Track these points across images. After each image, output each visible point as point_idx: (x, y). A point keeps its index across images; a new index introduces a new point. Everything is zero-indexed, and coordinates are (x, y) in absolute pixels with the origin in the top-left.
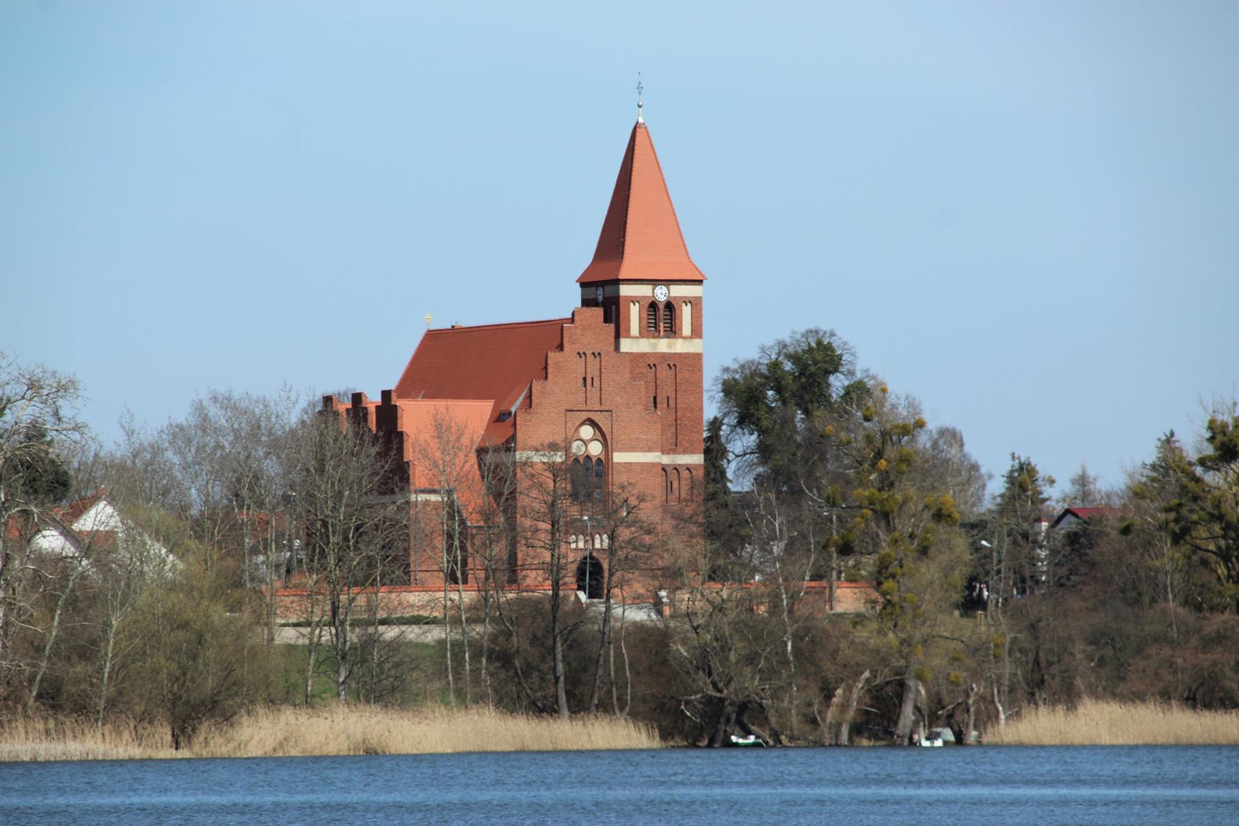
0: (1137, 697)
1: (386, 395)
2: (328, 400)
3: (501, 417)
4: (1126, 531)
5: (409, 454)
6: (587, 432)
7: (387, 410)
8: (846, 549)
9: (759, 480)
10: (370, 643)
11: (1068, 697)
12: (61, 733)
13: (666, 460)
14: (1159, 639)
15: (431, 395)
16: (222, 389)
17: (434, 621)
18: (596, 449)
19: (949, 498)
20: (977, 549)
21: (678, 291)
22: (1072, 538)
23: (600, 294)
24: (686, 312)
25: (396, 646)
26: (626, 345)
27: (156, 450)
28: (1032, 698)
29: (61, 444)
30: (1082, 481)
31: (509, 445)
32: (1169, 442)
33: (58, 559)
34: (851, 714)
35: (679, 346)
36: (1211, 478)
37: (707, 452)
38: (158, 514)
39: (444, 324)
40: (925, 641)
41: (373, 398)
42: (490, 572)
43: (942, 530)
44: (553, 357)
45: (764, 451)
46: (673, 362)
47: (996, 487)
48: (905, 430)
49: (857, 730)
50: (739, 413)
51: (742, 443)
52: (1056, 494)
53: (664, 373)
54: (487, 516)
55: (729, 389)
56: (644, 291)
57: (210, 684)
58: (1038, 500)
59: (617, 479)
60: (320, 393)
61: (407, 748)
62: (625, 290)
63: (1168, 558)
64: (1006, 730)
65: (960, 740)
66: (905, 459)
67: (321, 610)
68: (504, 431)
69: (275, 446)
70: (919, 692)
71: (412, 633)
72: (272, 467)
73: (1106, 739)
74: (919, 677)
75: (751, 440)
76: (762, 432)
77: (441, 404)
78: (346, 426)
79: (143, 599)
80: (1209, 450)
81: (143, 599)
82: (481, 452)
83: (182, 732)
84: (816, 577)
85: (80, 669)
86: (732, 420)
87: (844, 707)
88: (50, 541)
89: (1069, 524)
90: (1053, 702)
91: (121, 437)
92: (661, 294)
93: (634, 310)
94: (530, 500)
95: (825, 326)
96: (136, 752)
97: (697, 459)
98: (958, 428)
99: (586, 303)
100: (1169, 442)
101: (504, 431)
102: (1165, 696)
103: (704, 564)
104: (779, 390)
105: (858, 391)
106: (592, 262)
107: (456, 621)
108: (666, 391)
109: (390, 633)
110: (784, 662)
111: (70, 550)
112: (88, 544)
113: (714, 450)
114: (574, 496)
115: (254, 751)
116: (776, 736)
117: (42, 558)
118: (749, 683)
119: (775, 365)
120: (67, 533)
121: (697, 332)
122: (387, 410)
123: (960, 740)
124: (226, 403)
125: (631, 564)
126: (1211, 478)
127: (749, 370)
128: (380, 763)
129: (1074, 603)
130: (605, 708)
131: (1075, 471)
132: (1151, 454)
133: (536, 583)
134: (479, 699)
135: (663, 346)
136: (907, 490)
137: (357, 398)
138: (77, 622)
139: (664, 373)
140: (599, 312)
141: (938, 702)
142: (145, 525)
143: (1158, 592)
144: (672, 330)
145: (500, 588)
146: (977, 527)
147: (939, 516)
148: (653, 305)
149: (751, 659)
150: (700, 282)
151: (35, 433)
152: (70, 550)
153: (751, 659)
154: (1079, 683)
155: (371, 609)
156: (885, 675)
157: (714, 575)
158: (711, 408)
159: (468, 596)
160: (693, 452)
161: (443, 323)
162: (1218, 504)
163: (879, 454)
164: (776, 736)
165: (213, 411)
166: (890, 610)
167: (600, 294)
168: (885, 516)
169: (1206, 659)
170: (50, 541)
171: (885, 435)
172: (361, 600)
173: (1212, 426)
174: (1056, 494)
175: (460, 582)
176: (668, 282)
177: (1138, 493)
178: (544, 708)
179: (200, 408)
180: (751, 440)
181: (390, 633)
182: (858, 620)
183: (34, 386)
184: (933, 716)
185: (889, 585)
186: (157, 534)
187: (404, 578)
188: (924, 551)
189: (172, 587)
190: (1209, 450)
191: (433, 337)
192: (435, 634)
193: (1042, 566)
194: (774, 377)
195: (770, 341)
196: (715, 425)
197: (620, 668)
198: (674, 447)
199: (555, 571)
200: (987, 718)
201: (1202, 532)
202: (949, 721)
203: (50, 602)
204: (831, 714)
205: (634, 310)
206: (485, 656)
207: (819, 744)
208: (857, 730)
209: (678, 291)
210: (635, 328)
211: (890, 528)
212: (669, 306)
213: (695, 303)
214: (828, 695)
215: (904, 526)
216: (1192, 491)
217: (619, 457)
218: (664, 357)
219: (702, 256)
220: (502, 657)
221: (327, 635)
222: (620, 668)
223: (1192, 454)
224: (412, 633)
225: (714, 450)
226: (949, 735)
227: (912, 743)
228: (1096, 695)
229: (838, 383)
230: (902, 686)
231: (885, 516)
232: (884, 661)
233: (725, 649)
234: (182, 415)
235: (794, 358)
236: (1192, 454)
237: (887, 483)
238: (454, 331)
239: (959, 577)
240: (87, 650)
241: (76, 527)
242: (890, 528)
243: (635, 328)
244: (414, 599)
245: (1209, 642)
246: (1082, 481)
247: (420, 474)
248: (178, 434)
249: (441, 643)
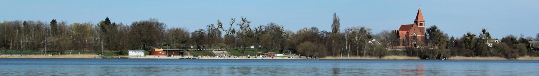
0: (460, 56)
1: (398, 30)
2: (393, 31)
3: (407, 32)
5: (400, 35)
6: (415, 33)
7: (398, 32)
8: (436, 43)
9: (429, 38)
10: (396, 50)
11: (455, 56)
12: (370, 57)
13: (421, 36)
14: (463, 51)
15: (402, 30)
16: (384, 30)
17: (401, 49)
18: (415, 35)
20: (447, 43)
21: (422, 22)
22: (456, 43)
24: (423, 24)
25: (398, 51)
26: (418, 26)
28: (452, 56)
29: (371, 34)
30: (457, 38)
31: (408, 34)
32: (465, 34)
33: (370, 43)
35: (423, 27)
37: (425, 35)
39: (403, 25)
40: (443, 51)
41: (397, 31)
42: (406, 45)
43: (444, 42)
44: (412, 27)
45: (430, 35)
46: (422, 28)
47: (450, 38)
48: (441, 34)
49: (437, 58)
50: (209, 56)
51: (428, 35)
52: (455, 39)
53: (421, 29)
54: (406, 40)
55: (427, 30)
56: (420, 22)
57: (382, 53)
58: (453, 39)
59: (417, 37)
60: (392, 30)
61: (399, 59)
62: (418, 22)
63: (464, 44)
64: (450, 58)
65: (446, 59)
66: (441, 36)
67: (392, 48)
68: (408, 33)
69: (388, 34)
70: (442, 55)
72: (388, 36)
74: (442, 54)
75: (429, 34)
76: (430, 34)
79: (377, 47)
80: (467, 35)
81: (377, 47)
82: (406, 35)
85: (372, 52)
86: (427, 33)
87: (436, 56)
88: (370, 42)
89: (456, 42)
90: (454, 56)
92: (421, 22)
93: (419, 24)
94: (410, 39)
95: (435, 25)
97: (424, 36)
99: (415, 23)
100: (465, 34)
101: (408, 33)
102: (463, 56)
103: (424, 45)
104: (431, 30)
105: (438, 31)
107: (403, 49)
108: (421, 30)
109: (397, 50)
110: (431, 52)
111: (371, 42)
112: (373, 42)
113: (426, 35)
116: (430, 59)
117: (369, 43)
118: (428, 54)
119: (431, 28)
120: (371, 41)
121: (424, 25)
122: (398, 32)
123: (446, 59)
124: (384, 31)
125: (418, 44)
128: (130, 39)
129: (455, 48)
130: (415, 56)
131: (456, 37)
132: (463, 36)
133: (410, 46)
134: (405, 55)
135: (421, 27)
136: (441, 39)
137: (395, 31)
138: (372, 48)
139: (421, 29)
140: (416, 24)
143: (463, 47)
144: (422, 25)
145: (407, 46)
146: (448, 42)
147: (444, 41)
148: (420, 23)
149: (428, 52)
150: (424, 21)
152: (371, 42)
154: (456, 55)
155: (396, 48)
156: (439, 54)
157: (425, 45)
158: (425, 32)
159: (404, 47)
163: (439, 36)
164: (430, 59)
165: (383, 32)
166: (440, 48)
168: (439, 41)
169: (467, 53)
170: (370, 42)
171: (440, 34)
172: (395, 47)
174: (455, 39)
176: (422, 21)
177: (461, 39)
178: (410, 56)
179: (382, 31)
180: (429, 34)
181: (397, 50)
182: (437, 49)
183: (368, 29)
184: (443, 57)
186: (379, 41)
187: (399, 45)
190: (467, 35)
191: (402, 26)
192: (401, 50)
194: (431, 29)
195: (430, 26)
196: (426, 33)
197: (417, 53)
198: (422, 35)
199: (411, 45)
202: (445, 58)
204: (434, 57)
205: (419, 24)
206: (334, 51)
207: (433, 59)
208: (437, 58)
211: (440, 42)
212: (422, 23)
213: (424, 23)
214: (434, 55)
215: (441, 42)
216: (466, 39)
217: (417, 36)
218: (421, 27)
219: (424, 19)
220: (407, 52)
222: (417, 53)
223: (466, 36)
224: (399, 50)
225: (426, 35)
226: (445, 59)
229: (436, 30)
230: (441, 55)
231: (439, 41)
232: (439, 53)
233: (426, 51)
235: (433, 28)
236: (466, 36)
237: (440, 38)
238: (404, 25)
239: (446, 46)
240: (372, 51)
241: (372, 41)
242: (440, 42)
244: (400, 47)
246: (457, 38)
247: (400, 37)
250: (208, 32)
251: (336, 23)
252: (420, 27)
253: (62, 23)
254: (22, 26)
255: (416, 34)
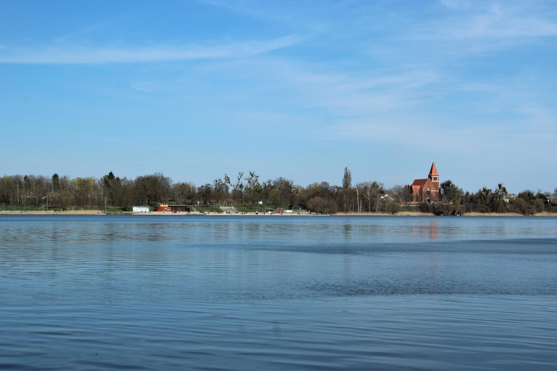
0: (476, 212)
1: (411, 185)
2: (406, 186)
3: (421, 187)
4: (476, 197)
5: (413, 190)
6: (428, 188)
7: (411, 187)
8: (451, 199)
9: (444, 193)
11: (470, 212)
13: (435, 191)
14: (478, 207)
16: (397, 184)
18: (429, 190)
19: (460, 195)
20: (462, 199)
21: (437, 176)
22: (471, 198)
23: (430, 177)
24: (437, 178)
25: (411, 206)
26: (432, 181)
27: (391, 190)
29: (383, 189)
30: (472, 193)
31: (422, 190)
33: (383, 199)
34: (451, 213)
35: (437, 181)
36: (483, 193)
38: (392, 195)
39: (416, 179)
41: (410, 185)
43: (459, 197)
44: (426, 182)
45: (444, 190)
46: (436, 183)
47: (465, 194)
48: (456, 189)
49: (451, 214)
51: (442, 190)
52: (470, 194)
53: (435, 184)
54: (419, 196)
55: (441, 185)
56: (434, 176)
57: (395, 209)
58: (469, 195)
59: (431, 192)
60: (405, 185)
62: (432, 176)
63: (479, 200)
64: (465, 214)
65: (460, 215)
67: (405, 203)
69: (401, 189)
71: (413, 205)
72: (401, 191)
73: (473, 215)
74: (457, 210)
75: (443, 189)
76: (444, 189)
77: (416, 186)
78: (407, 188)
79: (390, 202)
80: (483, 191)
81: (390, 202)
82: (419, 190)
83: (393, 213)
84: (448, 201)
86: (441, 188)
87: (450, 212)
88: (382, 197)
89: (471, 197)
90: (469, 212)
91: (388, 188)
92: (435, 177)
93: (433, 178)
94: (423, 194)
95: (450, 180)
96: (389, 215)
97: (438, 191)
98: (139, 176)
99: (429, 177)
103: (438, 200)
105: (452, 185)
106: (430, 174)
107: (416, 205)
108: (435, 185)
109: (411, 205)
110: (445, 208)
111: (384, 198)
112: (385, 197)
114: (427, 194)
115: (399, 215)
117: (381, 199)
118: (442, 210)
119: (445, 183)
120: (384, 196)
121: (438, 180)
122: (411, 187)
123: (460, 215)
124: (397, 186)
125: (432, 200)
126: (483, 193)
127: (443, 183)
129: (471, 203)
130: (429, 212)
133: (423, 201)
134: (418, 211)
135: (435, 181)
136: (456, 194)
137: (409, 185)
139: (435, 184)
140: (430, 178)
141: (458, 212)
142: (390, 196)
143: (478, 203)
144: (436, 180)
146: (462, 197)
147: (459, 196)
148: (434, 178)
149: (442, 208)
151: (381, 188)
152: (384, 198)
153: (442, 208)
156: (454, 210)
157: (439, 201)
158: (439, 187)
159: (418, 202)
160: (432, 192)
161: (416, 179)
162: (484, 195)
165: (396, 186)
166: (454, 204)
167: (430, 177)
168: (454, 196)
170: (382, 197)
171: (454, 189)
173: (483, 188)
174: (470, 194)
175: (369, 210)
177: (477, 194)
178: (424, 212)
179: (395, 186)
180: (443, 189)
181: (411, 205)
182: (452, 205)
183: (380, 184)
184: (458, 213)
185: (454, 202)
186: (391, 197)
187: (412, 201)
188: (457, 199)
189: (392, 201)
190: (483, 191)
191: (415, 181)
192: (414, 206)
193: (468, 200)
194: (445, 184)
196: (440, 188)
197: (431, 209)
198: (436, 190)
199: (425, 200)
200: (463, 213)
201: (482, 198)
202: (460, 214)
203: (382, 202)
204: (449, 213)
205: (433, 178)
207: (448, 215)
209: (437, 176)
210: (433, 180)
211: (454, 197)
213: (438, 178)
214: (449, 211)
215: (456, 197)
216: (482, 194)
217: (431, 191)
219: (439, 173)
220: (420, 208)
221: (405, 206)
222: (431, 209)
224: (413, 205)
225: (440, 190)
226: (459, 215)
227: (456, 216)
228: (472, 211)
229: (451, 185)
230: (455, 211)
231: (454, 196)
234: (393, 187)
235: (447, 182)
237: (454, 193)
238: (417, 180)
240: (385, 206)
241: (385, 196)
242: (454, 197)
243: (433, 180)
244: (413, 203)
245: (483, 207)
246: (472, 193)
247: (414, 192)
248: (394, 188)
249: (415, 206)
250: (215, 187)
251: (347, 178)
252: (434, 181)
253: (64, 177)
254: (23, 180)
255: (430, 189)
